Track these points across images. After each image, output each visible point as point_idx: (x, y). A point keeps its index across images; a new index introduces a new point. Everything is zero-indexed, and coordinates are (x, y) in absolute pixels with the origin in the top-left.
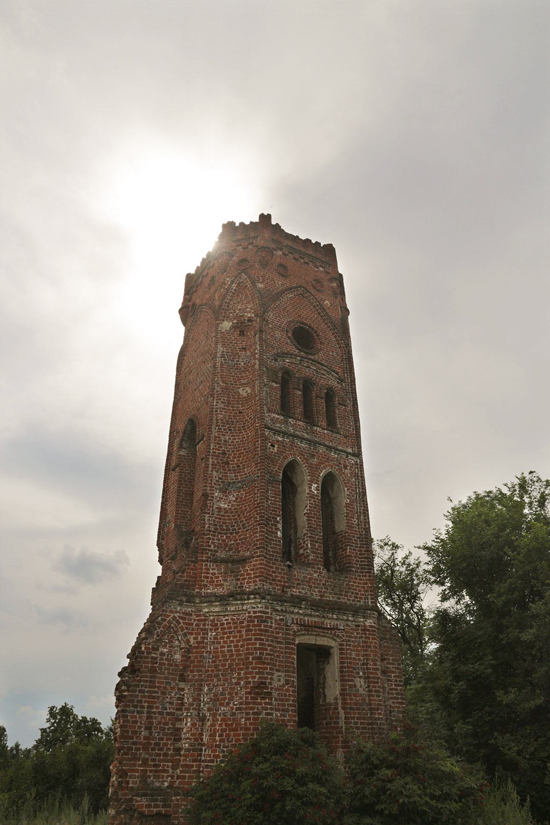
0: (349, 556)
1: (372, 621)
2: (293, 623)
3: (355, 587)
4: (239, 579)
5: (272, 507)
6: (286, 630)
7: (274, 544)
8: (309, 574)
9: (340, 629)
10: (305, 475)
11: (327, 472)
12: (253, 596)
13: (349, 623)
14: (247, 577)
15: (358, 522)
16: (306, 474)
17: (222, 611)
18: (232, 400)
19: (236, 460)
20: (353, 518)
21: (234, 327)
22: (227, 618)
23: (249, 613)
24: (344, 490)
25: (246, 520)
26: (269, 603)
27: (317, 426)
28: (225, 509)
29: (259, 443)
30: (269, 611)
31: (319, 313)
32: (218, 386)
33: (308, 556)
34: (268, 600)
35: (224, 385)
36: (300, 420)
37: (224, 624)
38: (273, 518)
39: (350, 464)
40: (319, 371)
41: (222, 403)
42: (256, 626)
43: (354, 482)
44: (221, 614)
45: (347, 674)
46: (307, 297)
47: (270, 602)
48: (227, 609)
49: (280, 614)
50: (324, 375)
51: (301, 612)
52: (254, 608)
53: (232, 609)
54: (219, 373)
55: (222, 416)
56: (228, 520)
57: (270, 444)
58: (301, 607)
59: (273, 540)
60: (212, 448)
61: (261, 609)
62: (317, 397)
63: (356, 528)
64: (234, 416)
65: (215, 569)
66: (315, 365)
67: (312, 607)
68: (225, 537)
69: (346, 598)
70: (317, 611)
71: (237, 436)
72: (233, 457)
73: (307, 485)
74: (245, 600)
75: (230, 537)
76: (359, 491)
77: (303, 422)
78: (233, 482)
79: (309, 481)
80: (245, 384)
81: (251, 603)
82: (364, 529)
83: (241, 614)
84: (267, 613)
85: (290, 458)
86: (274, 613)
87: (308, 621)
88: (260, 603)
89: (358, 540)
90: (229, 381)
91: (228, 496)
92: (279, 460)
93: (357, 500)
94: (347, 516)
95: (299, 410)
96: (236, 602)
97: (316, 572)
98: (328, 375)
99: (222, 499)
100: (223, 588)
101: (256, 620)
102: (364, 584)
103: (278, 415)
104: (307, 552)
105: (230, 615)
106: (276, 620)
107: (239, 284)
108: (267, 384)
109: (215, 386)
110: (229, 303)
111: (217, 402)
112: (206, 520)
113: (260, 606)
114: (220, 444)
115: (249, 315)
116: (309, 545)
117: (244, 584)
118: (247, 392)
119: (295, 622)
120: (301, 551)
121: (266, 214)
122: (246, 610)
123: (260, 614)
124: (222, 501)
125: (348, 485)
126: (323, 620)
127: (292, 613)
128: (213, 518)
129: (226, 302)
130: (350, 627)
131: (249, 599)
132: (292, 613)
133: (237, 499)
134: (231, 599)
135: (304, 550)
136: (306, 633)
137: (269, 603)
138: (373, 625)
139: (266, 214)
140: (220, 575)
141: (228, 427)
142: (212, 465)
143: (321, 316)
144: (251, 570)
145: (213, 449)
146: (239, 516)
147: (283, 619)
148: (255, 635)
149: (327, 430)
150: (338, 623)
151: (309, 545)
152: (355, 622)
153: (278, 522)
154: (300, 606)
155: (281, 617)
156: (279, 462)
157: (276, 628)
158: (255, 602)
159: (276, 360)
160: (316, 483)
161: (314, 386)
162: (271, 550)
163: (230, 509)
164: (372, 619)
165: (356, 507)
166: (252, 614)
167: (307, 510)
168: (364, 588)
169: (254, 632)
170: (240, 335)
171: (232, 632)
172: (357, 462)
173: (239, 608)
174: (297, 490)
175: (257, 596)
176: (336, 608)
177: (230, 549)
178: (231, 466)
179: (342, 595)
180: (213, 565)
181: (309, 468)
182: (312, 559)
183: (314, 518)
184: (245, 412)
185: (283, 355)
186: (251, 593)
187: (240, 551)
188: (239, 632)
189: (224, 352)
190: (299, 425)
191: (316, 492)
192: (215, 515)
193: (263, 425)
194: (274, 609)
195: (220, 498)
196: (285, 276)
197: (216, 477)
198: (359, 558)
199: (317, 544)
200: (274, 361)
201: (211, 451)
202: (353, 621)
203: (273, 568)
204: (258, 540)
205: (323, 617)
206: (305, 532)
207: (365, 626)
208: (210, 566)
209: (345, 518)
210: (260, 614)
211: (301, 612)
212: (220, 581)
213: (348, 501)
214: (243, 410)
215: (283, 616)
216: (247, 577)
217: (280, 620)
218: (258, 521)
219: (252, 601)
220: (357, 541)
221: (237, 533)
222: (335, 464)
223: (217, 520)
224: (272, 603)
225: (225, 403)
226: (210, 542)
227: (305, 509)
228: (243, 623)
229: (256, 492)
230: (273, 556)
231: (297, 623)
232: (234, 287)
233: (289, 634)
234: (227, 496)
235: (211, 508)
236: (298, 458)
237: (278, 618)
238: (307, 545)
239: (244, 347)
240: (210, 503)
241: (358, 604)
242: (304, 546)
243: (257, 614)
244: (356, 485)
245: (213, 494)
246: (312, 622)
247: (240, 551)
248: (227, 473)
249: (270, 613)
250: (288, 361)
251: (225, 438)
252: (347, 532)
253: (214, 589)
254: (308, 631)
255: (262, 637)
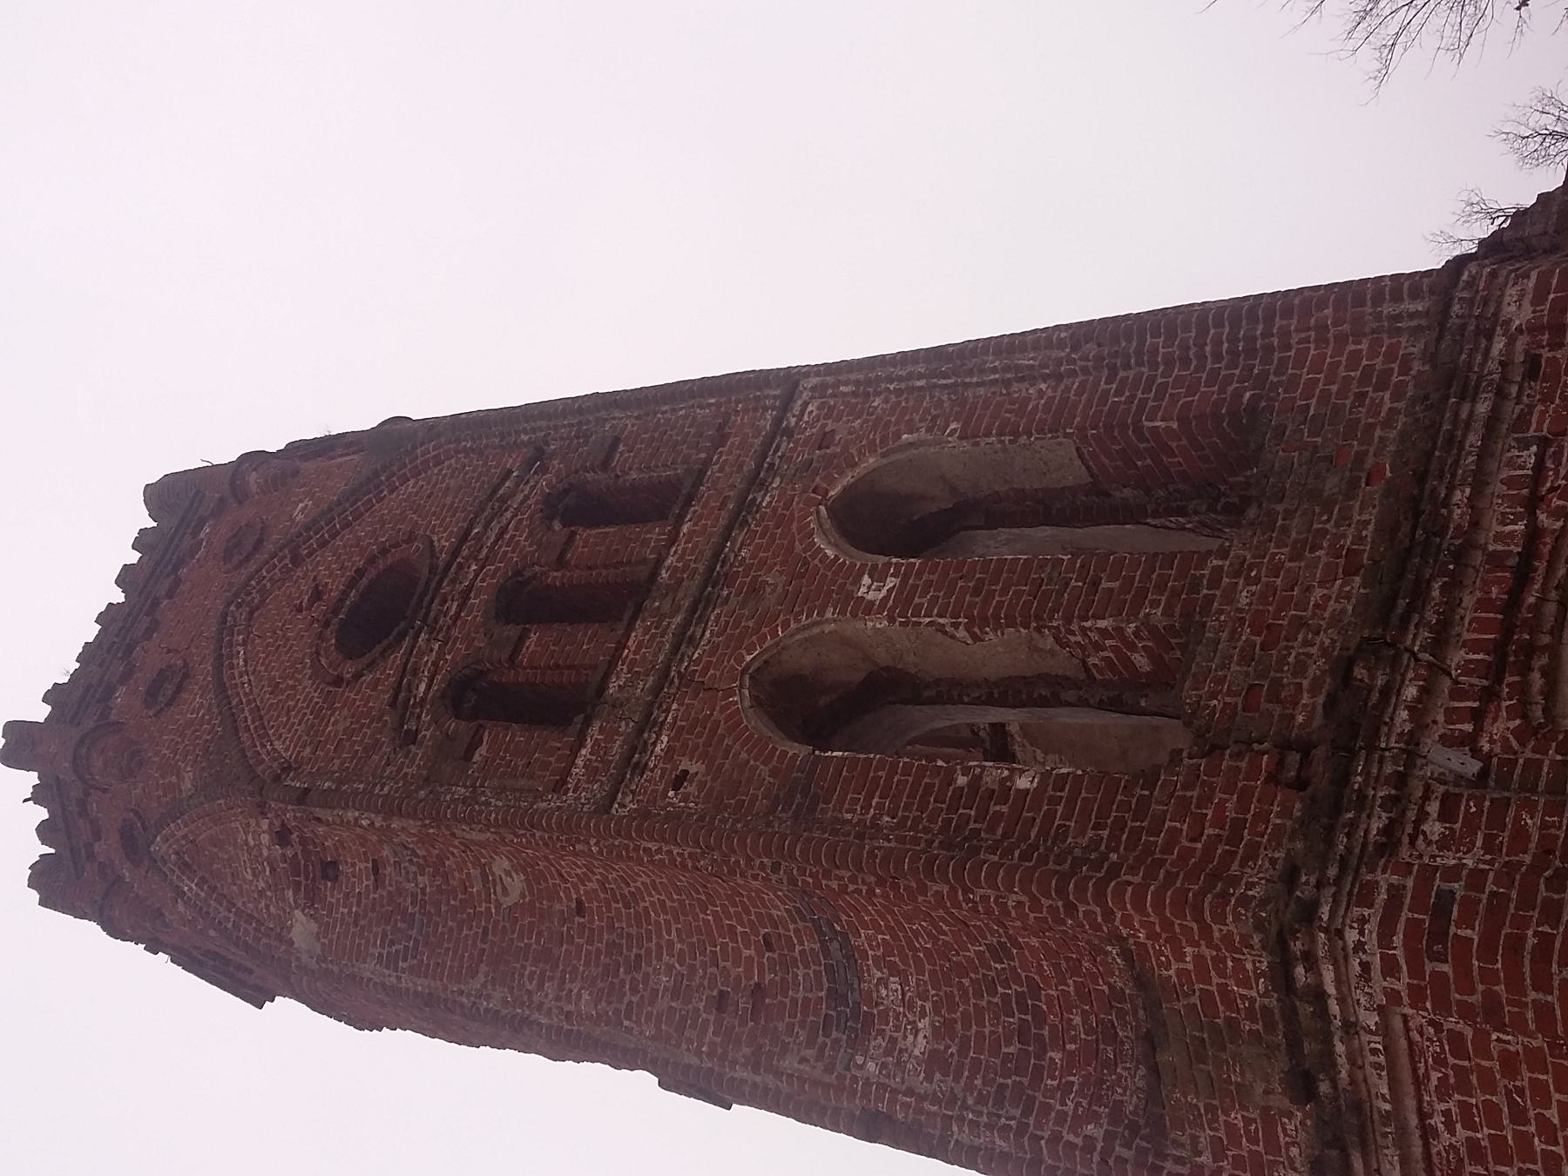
0: (1182, 420)
1: (1512, 292)
2: (1469, 742)
3: (1334, 388)
4: (1228, 1020)
5: (907, 807)
6: (1503, 783)
7: (1068, 816)
8: (1233, 631)
9: (1539, 467)
10: (816, 630)
11: (828, 525)
12: (1300, 970)
13: (1511, 410)
14: (1216, 980)
15: (1045, 378)
16: (816, 624)
17: (1402, 1142)
18: (537, 942)
19: (746, 953)
20: (1029, 399)
21: (311, 899)
22: (1437, 1121)
23: (1394, 997)
24: (911, 445)
25: (974, 941)
26: (1338, 881)
27: (659, 562)
28: (935, 1031)
29: (653, 846)
30: (1385, 880)
31: (323, 544)
32: (488, 998)
33: (1153, 630)
34: (1319, 885)
35: (483, 968)
36: (622, 645)
37: (1472, 1144)
38: (953, 808)
39: (818, 416)
40: (485, 551)
41: (540, 987)
42: (1463, 969)
43: (886, 401)
44: (1417, 1150)
45: (433, 509)
46: (264, 593)
47: (1332, 872)
48: (1386, 1118)
49: (1411, 815)
50: (503, 531)
51: (1411, 692)
52: (1366, 966)
53: (1385, 1091)
54: (445, 989)
55: (586, 996)
56: (981, 1024)
57: (671, 793)
58: (1386, 692)
59: (1052, 815)
60: (695, 1061)
61: (1372, 927)
62: (561, 563)
63: (1068, 389)
64: (590, 942)
65: (1195, 1139)
66: (460, 566)
67: (1395, 620)
68: (1057, 1056)
69: (1378, 433)
70: (1419, 594)
71: (660, 936)
72: (736, 964)
73: (860, 625)
74: (1323, 1014)
75: (1053, 1027)
76: (920, 376)
77: (630, 628)
78: (832, 980)
79: (843, 612)
80: (484, 877)
81: (1338, 982)
82: (1074, 349)
83: (1410, 1042)
84: (1395, 893)
85: (742, 699)
86: (1404, 853)
87: (1474, 646)
88: (1340, 934)
89: (1122, 374)
90: (474, 944)
91: (886, 1011)
92: (737, 754)
93: (955, 385)
94: (1016, 434)
95: (587, 643)
96: (1342, 1061)
97: (1230, 595)
98: (508, 515)
99: (893, 1041)
100: (1282, 1114)
101: (1429, 967)
102: (1322, 341)
103: (582, 745)
104: (1136, 634)
105: (1420, 1101)
106: (1444, 844)
107: (186, 867)
108: (473, 785)
109: (487, 1010)
110: (239, 913)
111: (540, 1008)
112: (977, 1142)
113: (1352, 936)
114: (684, 1019)
115: (265, 839)
116: (1102, 624)
117: (1252, 1000)
118: (508, 874)
119: (1468, 727)
120: (1141, 661)
121: (3, 741)
122: (1381, 1010)
123: (1398, 940)
124: (901, 1044)
125: (892, 429)
126: (1478, 558)
127: (1412, 740)
128: (970, 1102)
129: (236, 925)
130: (1531, 407)
131: (1319, 995)
132: (1412, 740)
133: (893, 970)
134: (1324, 1088)
135: (1133, 648)
136: (1545, 660)
137: (1338, 881)
138: (1531, 283)
139: (3, 741)
140: (1222, 1118)
141: (628, 972)
142: (756, 1070)
143: (333, 537)
144: (1181, 957)
145: (699, 1053)
146: (960, 970)
147: (1445, 798)
148: (1515, 984)
149: (680, 520)
150: (1504, 474)
151: (1102, 624)
152: (1505, 379)
153: (976, 781)
154: (1375, 696)
155: (1433, 808)
156: (744, 755)
157: (1489, 846)
158: (1335, 963)
159: (412, 738)
160: (857, 582)
161: (527, 573)
162: (1090, 833)
163: (936, 1011)
164: (1503, 289)
165: (982, 391)
166: (1401, 985)
167: (956, 626)
168: (1341, 340)
169: (1501, 988)
170: (335, 879)
171: (1512, 1104)
172: (813, 389)
173: (1374, 1052)
174: (887, 669)
175: (1297, 947)
176: (1416, 492)
177: (1110, 1035)
178: (768, 977)
179: (1360, 458)
180: (1177, 1144)
181: (797, 609)
182: (1168, 612)
183: (991, 594)
184: (575, 886)
185: (400, 700)
186: (1282, 978)
187: (1110, 986)
188: (1509, 1063)
189: (380, 955)
190: (639, 647)
191: (891, 582)
192: (959, 1088)
193: (588, 824)
194: (1381, 849)
195: (888, 1053)
196: (186, 676)
197: (803, 1060)
198: (1201, 367)
199: (1105, 584)
200: (413, 747)
201: (707, 1064)
202: (1501, 394)
203: (1174, 834)
204: (1036, 906)
205: (1459, 555)
206: (1049, 642)
207: (1533, 329)
208: (1179, 1161)
209: (1023, 440)
210: (1398, 940)
211: (1411, 692)
212: (1248, 1121)
213: (953, 426)
214: (569, 898)
215: (1426, 798)
216: (1216, 980)
217: (1446, 815)
218: (953, 889)
219: (1328, 976)
220: (1124, 380)
221: (1035, 990)
222: (804, 491)
223: (978, 1082)
224: (1343, 863)
225: (543, 973)
226: (1071, 1138)
227: (953, 637)
228: (1456, 1039)
229: (835, 885)
230: (1120, 825)
231: (1477, 716)
232: (190, 889)
233: (1533, 766)
234: (884, 1016)
235: (926, 1105)
236: (749, 658)
237: (1434, 828)
238: (1104, 633)
239: (370, 865)
240: (906, 1106)
241: (1417, 366)
242: (1114, 649)
243: (1399, 953)
244: (899, 392)
245: (867, 1083)
246: (1483, 626)
247: (1110, 986)
248: (794, 1001)
249: (1395, 879)
250: (423, 687)
251: (666, 989)
252: (1081, 429)
253: (1291, 1161)
254: (1530, 650)
255: (1531, 941)
